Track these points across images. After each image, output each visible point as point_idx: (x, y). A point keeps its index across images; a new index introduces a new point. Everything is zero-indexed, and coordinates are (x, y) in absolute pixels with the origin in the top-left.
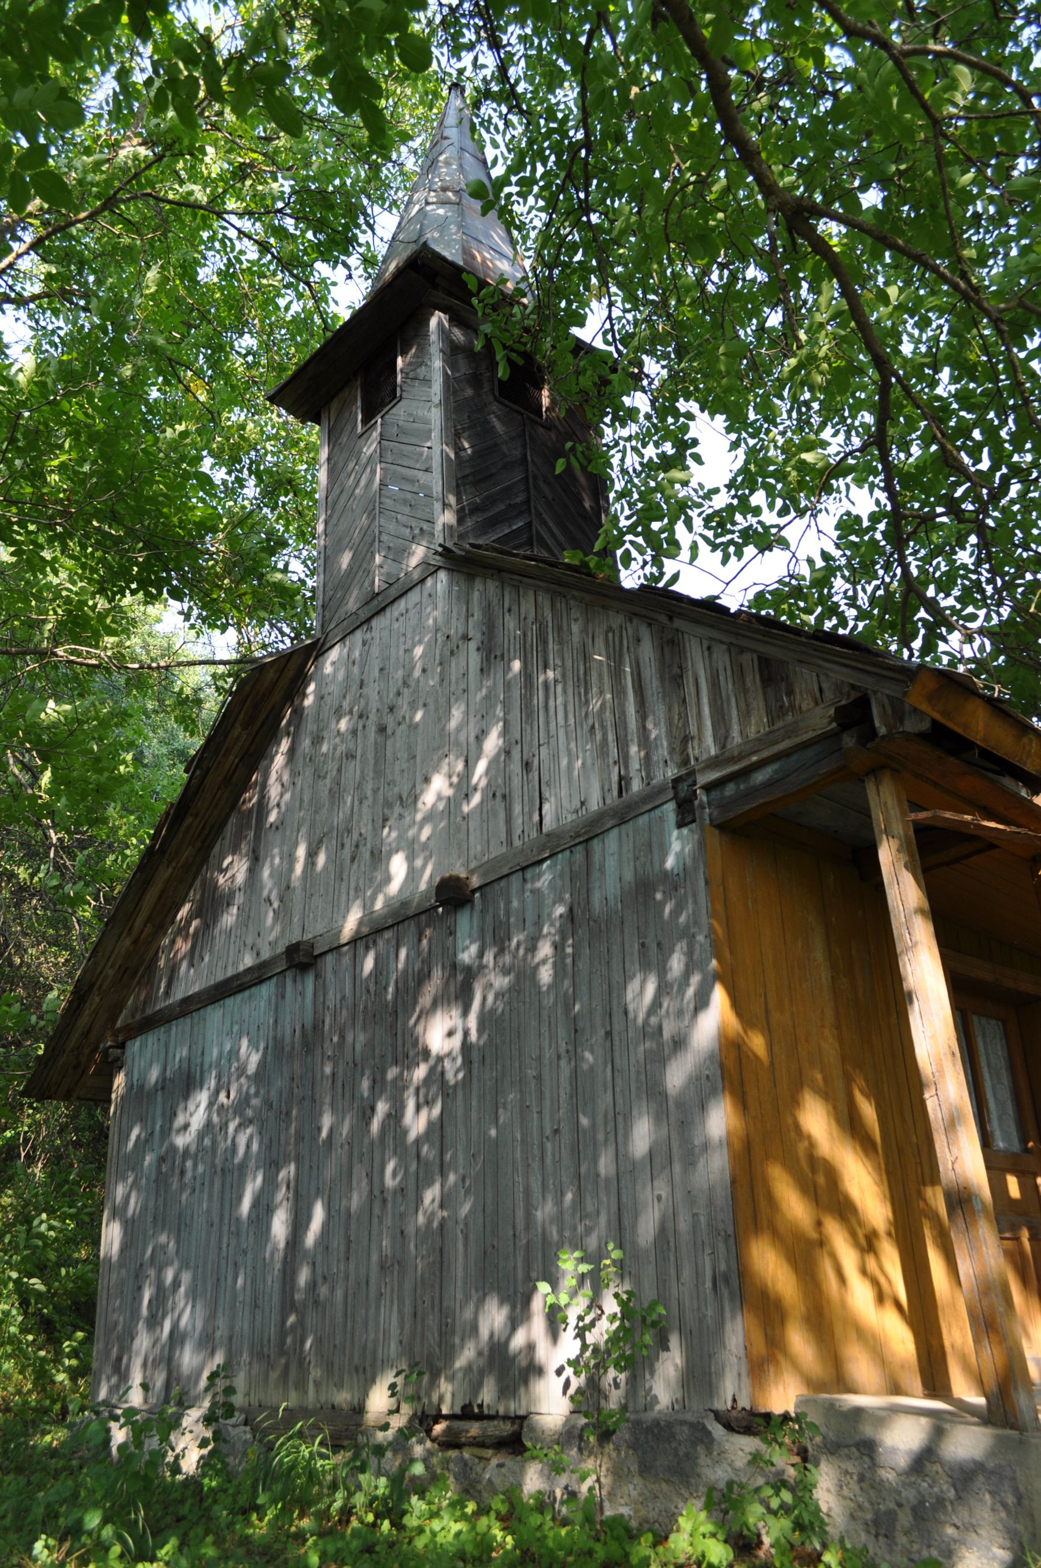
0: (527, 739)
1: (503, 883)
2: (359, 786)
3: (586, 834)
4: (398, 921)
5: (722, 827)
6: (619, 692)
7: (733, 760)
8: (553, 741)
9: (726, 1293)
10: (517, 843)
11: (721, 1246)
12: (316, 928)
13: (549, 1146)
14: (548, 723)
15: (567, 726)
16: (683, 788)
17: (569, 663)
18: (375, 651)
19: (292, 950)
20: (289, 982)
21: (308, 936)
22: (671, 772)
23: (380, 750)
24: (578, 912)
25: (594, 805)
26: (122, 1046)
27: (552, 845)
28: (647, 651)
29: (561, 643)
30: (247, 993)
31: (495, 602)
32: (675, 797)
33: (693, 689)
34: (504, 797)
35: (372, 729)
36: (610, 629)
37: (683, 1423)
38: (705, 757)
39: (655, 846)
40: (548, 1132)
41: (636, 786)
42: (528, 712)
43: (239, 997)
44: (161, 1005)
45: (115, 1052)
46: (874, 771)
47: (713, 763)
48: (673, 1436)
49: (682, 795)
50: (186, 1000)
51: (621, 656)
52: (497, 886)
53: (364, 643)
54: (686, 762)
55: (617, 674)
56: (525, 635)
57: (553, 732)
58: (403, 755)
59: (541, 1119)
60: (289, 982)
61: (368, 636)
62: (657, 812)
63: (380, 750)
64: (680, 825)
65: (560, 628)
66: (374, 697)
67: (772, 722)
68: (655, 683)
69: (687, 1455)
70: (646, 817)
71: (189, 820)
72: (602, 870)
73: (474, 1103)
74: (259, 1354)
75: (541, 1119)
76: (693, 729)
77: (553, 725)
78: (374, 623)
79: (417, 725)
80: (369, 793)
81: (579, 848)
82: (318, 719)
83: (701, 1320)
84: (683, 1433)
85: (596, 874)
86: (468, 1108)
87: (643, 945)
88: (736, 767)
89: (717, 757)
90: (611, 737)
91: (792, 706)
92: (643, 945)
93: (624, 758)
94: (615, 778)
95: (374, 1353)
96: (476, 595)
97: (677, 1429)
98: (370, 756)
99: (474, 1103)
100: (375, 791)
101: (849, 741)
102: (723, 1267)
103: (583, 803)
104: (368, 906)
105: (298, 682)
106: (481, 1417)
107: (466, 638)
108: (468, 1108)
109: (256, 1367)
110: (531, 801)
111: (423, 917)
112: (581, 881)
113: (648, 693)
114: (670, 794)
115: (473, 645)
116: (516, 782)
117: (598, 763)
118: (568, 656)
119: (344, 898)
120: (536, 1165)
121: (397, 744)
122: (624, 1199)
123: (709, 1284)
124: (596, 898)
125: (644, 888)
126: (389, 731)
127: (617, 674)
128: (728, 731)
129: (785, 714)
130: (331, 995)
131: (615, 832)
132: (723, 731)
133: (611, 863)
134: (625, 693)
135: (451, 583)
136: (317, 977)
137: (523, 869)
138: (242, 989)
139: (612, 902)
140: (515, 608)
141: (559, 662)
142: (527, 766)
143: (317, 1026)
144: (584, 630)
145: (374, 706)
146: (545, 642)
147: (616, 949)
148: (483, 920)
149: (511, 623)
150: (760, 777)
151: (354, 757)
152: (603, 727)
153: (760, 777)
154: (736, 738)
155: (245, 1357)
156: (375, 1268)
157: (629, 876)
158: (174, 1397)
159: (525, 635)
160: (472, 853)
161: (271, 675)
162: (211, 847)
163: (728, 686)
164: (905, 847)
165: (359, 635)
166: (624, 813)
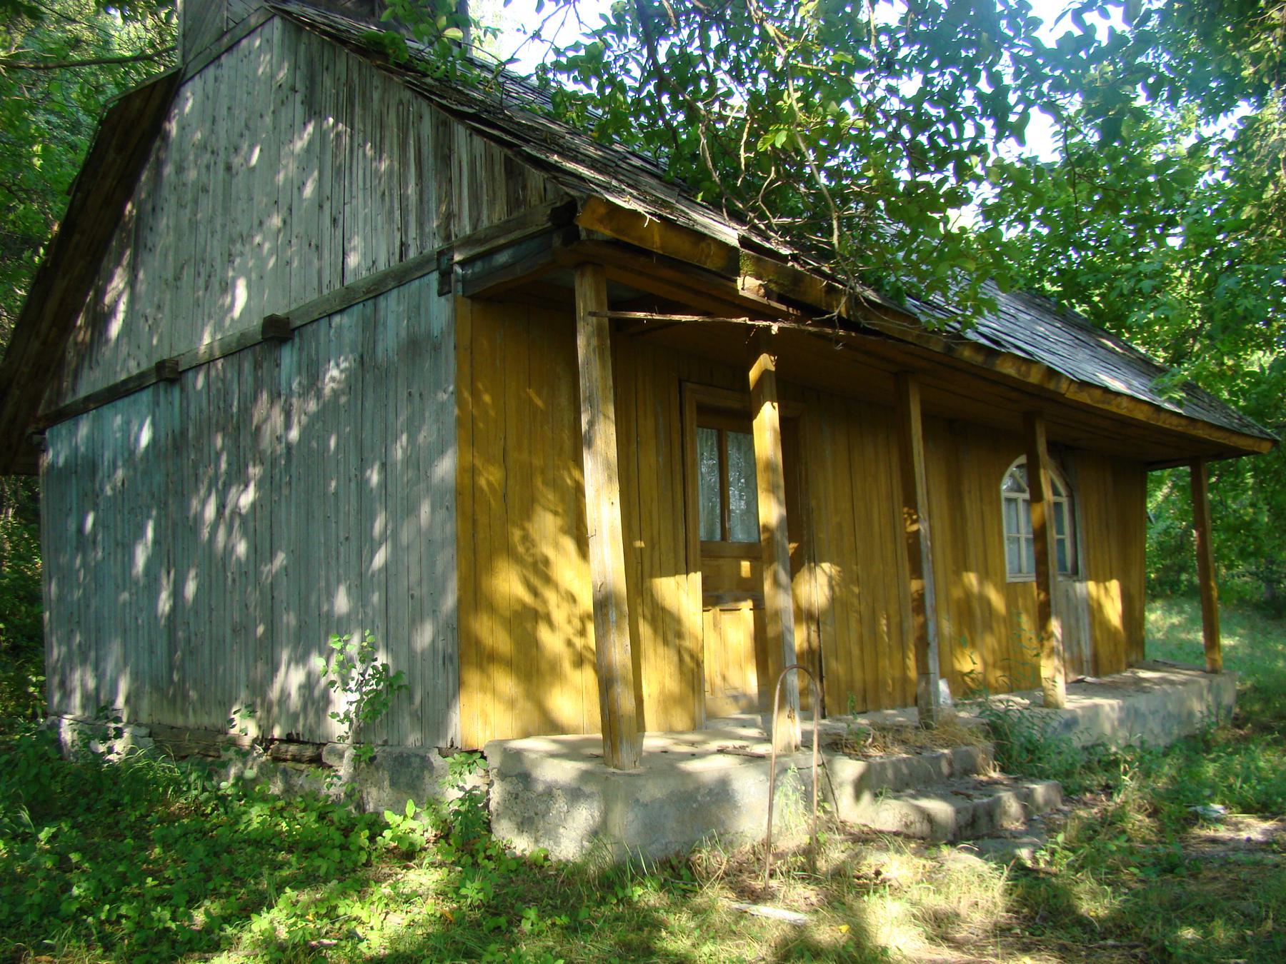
0: (335, 196)
1: (315, 325)
2: (211, 220)
3: (376, 289)
4: (234, 351)
5: (474, 298)
6: (403, 163)
7: (480, 242)
8: (354, 202)
9: (450, 669)
10: (326, 292)
11: (449, 634)
12: (181, 348)
13: (342, 549)
14: (351, 184)
15: (365, 189)
16: (444, 260)
17: (369, 129)
18: (224, 88)
19: (161, 366)
20: (162, 392)
21: (175, 354)
22: (437, 244)
23: (227, 186)
24: (367, 359)
25: (382, 266)
26: (42, 432)
27: (348, 299)
28: (427, 128)
29: (364, 108)
30: (132, 398)
31: (316, 59)
32: (438, 268)
33: (457, 169)
34: (317, 247)
35: (221, 166)
36: (401, 102)
37: (417, 755)
38: (461, 236)
39: (423, 310)
40: (342, 539)
41: (412, 254)
42: (338, 172)
43: (126, 400)
44: (69, 400)
45: (36, 438)
46: (580, 266)
47: (468, 242)
48: (409, 764)
49: (443, 267)
50: (88, 399)
51: (408, 129)
52: (310, 328)
53: (216, 79)
54: (448, 237)
55: (403, 147)
56: (338, 94)
57: (354, 193)
58: (243, 195)
59: (337, 528)
60: (162, 392)
61: (219, 72)
62: (425, 279)
63: (227, 186)
64: (441, 294)
65: (364, 94)
66: (222, 134)
67: (510, 212)
68: (431, 161)
69: (418, 776)
70: (417, 282)
71: (77, 237)
72: (385, 324)
73: (293, 510)
74: (156, 687)
75: (337, 528)
76: (455, 207)
77: (354, 186)
78: (223, 59)
79: (253, 169)
80: (219, 228)
81: (370, 303)
82: (180, 150)
83: (435, 687)
84: (416, 762)
85: (381, 328)
86: (289, 513)
87: (410, 394)
88: (482, 249)
89: (469, 237)
90: (396, 205)
91: (524, 200)
92: (410, 394)
93: (404, 229)
94: (398, 244)
95: (231, 692)
96: (303, 47)
97: (413, 759)
98: (220, 192)
99: (293, 510)
100: (224, 226)
101: (557, 241)
102: (450, 651)
103: (374, 262)
104: (219, 327)
105: (163, 113)
106: (298, 741)
107: (293, 90)
108: (289, 513)
109: (155, 695)
110: (336, 257)
111: (258, 348)
112: (371, 326)
113: (425, 168)
114: (434, 266)
115: (299, 97)
116: (327, 238)
117: (386, 227)
118: (368, 121)
119: (200, 323)
120: (333, 563)
121: (239, 182)
122: (390, 595)
123: (441, 662)
124: (380, 349)
125: (415, 347)
126: (234, 171)
127: (403, 147)
128: (479, 213)
129: (519, 207)
130: (192, 406)
131: (395, 292)
132: (475, 214)
133: (391, 320)
134: (409, 166)
135: (284, 30)
136: (182, 390)
137: (330, 316)
138: (128, 393)
139: (390, 354)
140: (331, 66)
141: (361, 127)
142: (334, 221)
143: (184, 432)
144: (382, 100)
145: (223, 143)
146: (353, 106)
147: (391, 394)
148: (300, 355)
149: (328, 82)
150: (502, 258)
151: (207, 191)
152: (391, 195)
153: (502, 258)
154: (485, 223)
155: (147, 688)
156: (229, 631)
157: (403, 334)
158: (100, 709)
159: (338, 94)
160: (293, 294)
161: (137, 103)
162: (100, 260)
163: (482, 174)
164: (599, 331)
165: (211, 72)
166: (401, 276)
